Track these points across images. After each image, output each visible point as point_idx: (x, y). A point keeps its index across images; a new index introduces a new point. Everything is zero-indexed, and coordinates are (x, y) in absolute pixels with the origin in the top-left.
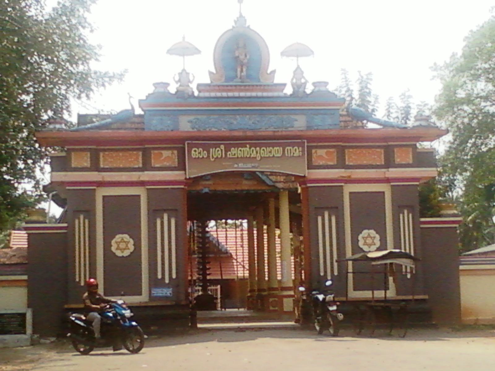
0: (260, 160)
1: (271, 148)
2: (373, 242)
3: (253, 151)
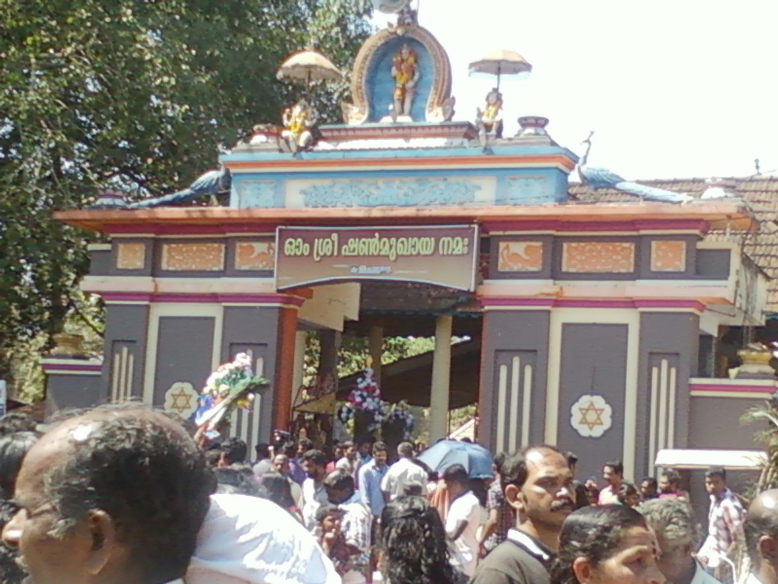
0: (395, 261)
1: (416, 239)
2: (599, 418)
3: (384, 243)
